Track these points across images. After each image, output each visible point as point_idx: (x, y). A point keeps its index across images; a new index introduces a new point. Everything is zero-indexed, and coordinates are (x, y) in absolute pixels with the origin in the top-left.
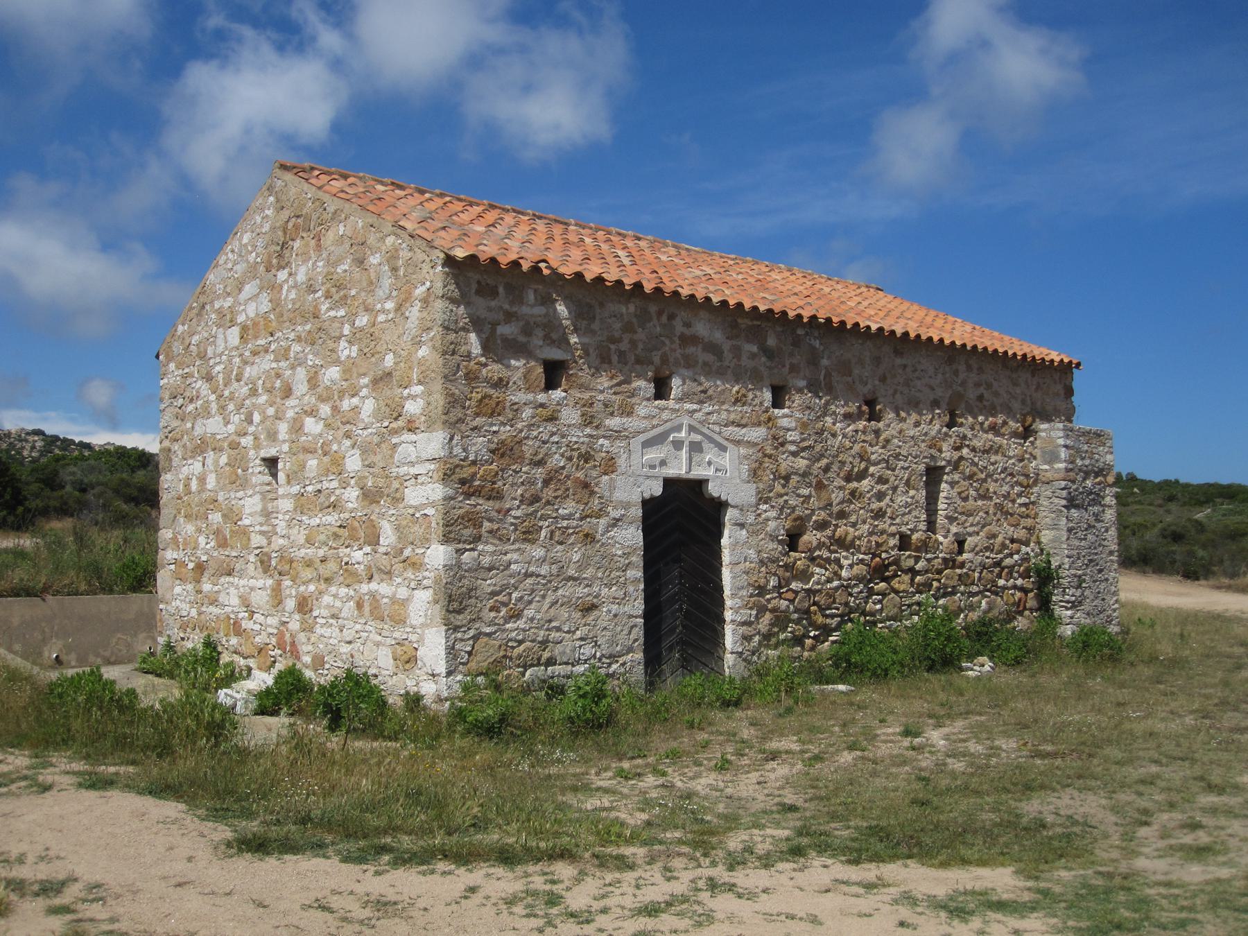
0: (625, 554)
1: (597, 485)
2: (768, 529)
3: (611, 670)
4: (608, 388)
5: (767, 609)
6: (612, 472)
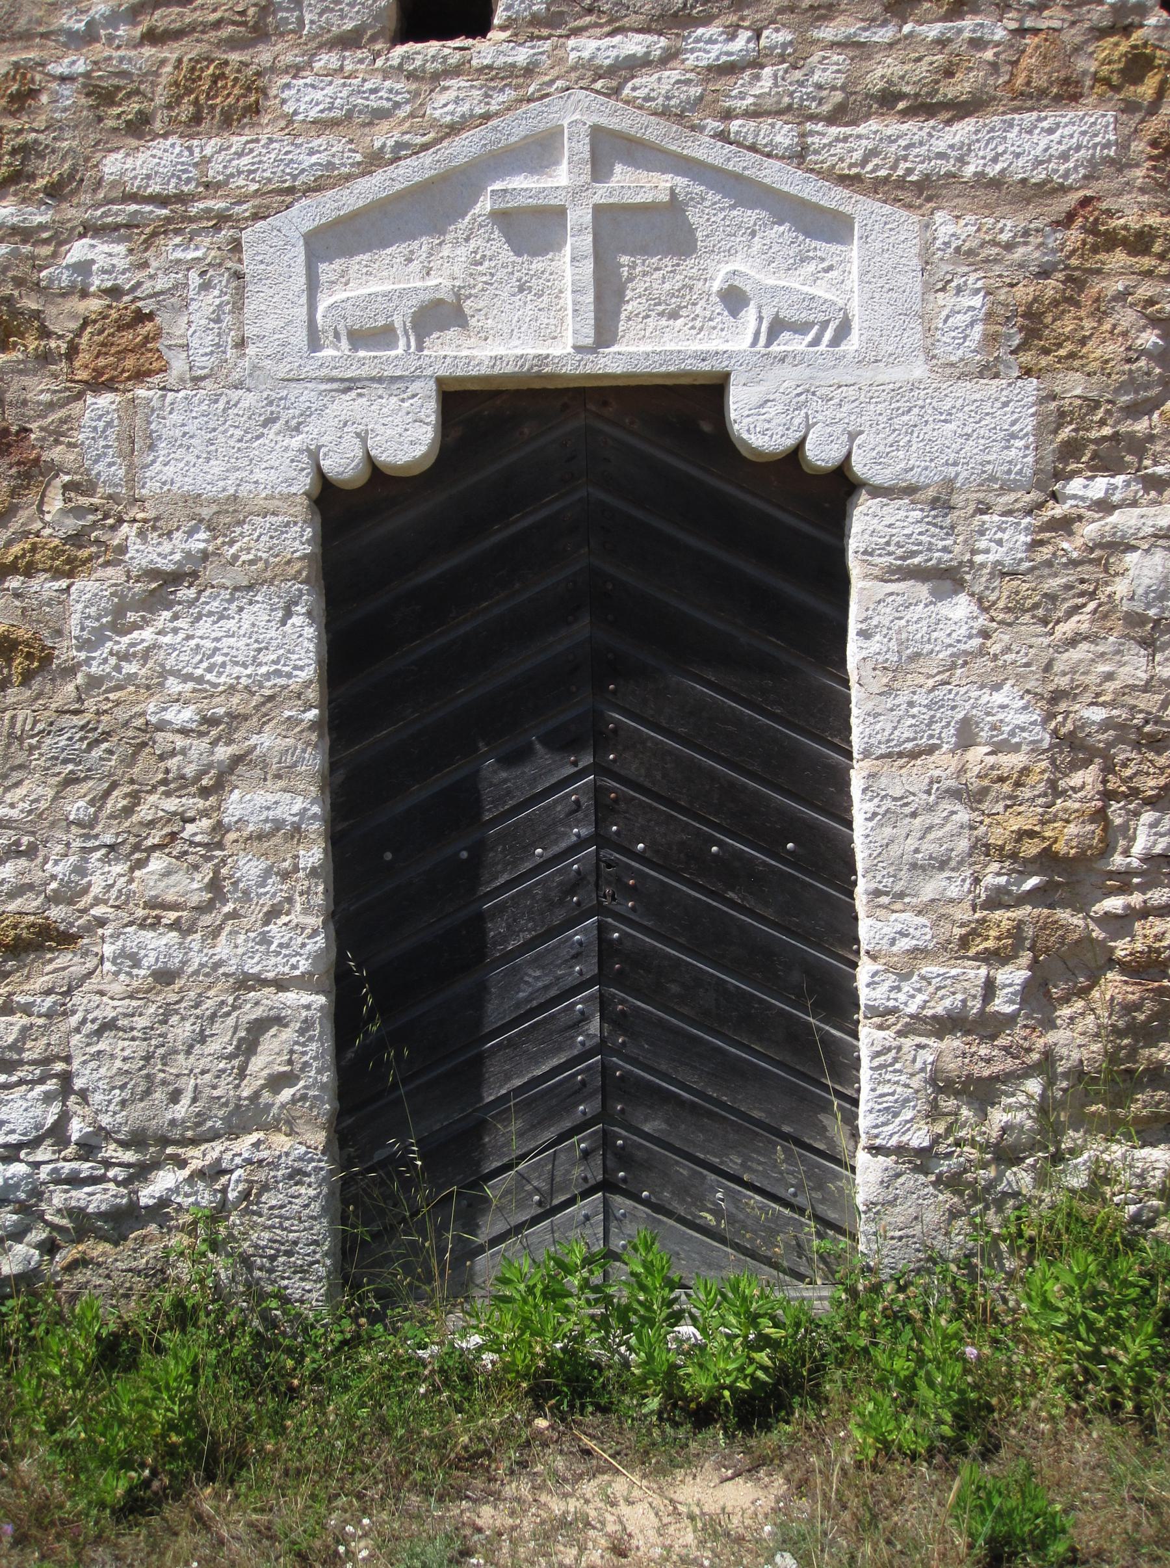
0: (213, 722)
1: (57, 435)
2: (1120, 588)
3: (147, 1195)
4: (113, 19)
5: (1111, 963)
6: (140, 375)
